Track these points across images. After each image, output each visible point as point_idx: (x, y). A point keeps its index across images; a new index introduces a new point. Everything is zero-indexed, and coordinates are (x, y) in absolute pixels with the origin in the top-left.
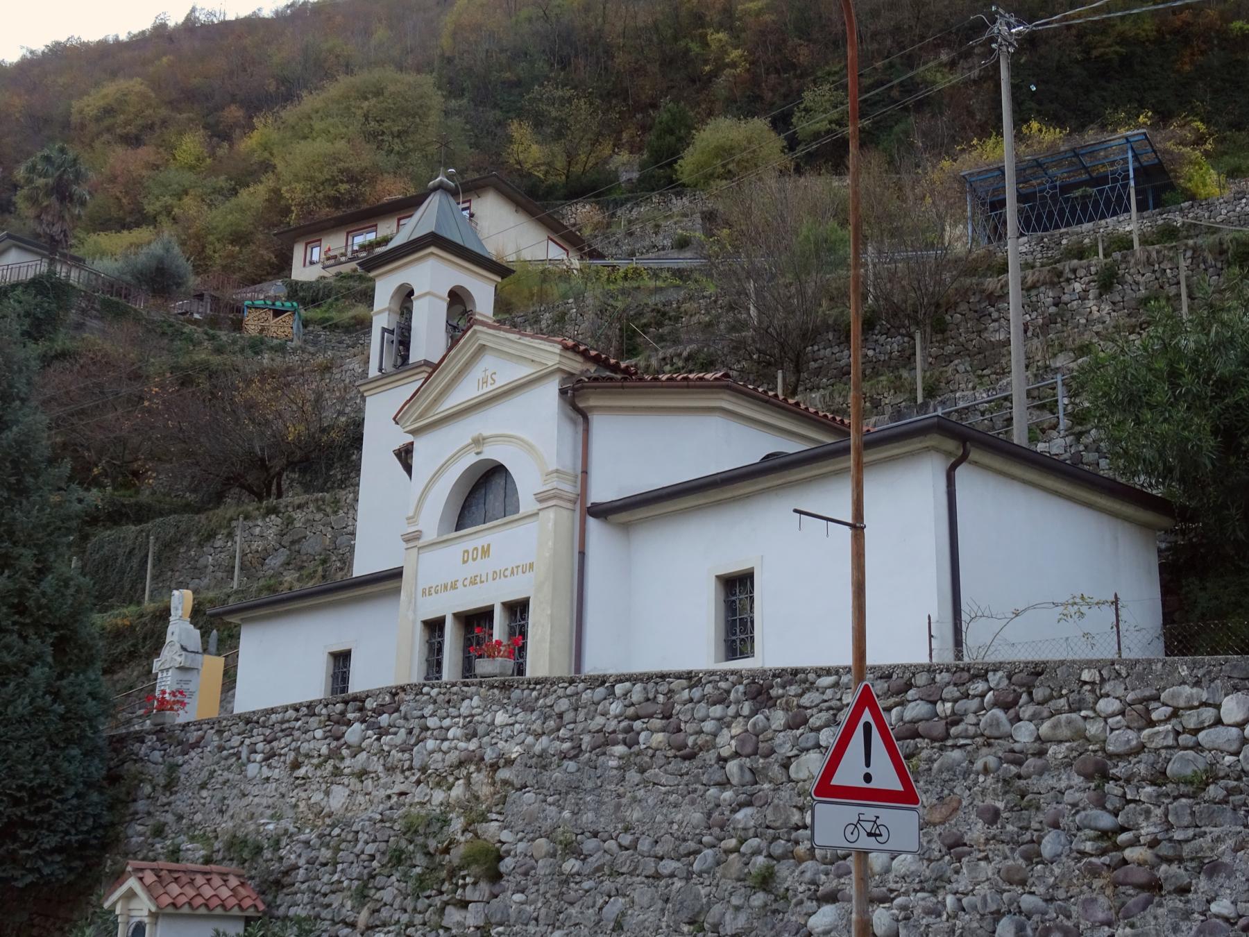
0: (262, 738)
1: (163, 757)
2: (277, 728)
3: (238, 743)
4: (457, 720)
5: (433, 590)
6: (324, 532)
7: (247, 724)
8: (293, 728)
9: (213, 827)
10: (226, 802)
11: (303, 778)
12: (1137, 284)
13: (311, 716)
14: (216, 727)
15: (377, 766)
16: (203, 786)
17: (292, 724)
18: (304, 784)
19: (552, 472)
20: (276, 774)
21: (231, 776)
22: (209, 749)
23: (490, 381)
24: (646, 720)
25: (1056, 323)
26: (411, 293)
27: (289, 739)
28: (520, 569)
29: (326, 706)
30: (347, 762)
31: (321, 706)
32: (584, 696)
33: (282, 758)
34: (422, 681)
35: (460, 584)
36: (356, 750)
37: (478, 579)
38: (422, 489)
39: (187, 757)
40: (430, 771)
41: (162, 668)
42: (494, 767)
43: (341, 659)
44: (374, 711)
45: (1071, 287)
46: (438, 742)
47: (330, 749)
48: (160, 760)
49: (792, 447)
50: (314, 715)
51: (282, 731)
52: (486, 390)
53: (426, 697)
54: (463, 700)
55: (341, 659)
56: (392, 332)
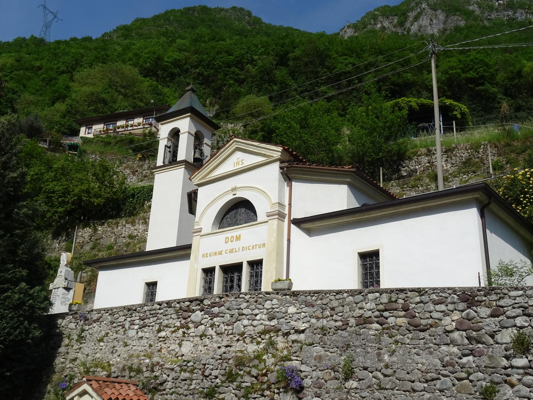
0: (138, 318)
1: (76, 326)
2: (148, 313)
3: (123, 320)
4: (262, 310)
5: (208, 255)
6: (111, 236)
7: (129, 311)
8: (157, 313)
9: (108, 360)
10: (115, 348)
11: (164, 338)
12: (462, 157)
13: (169, 308)
14: (110, 312)
15: (211, 332)
16: (101, 340)
17: (157, 312)
18: (164, 341)
19: (276, 203)
20: (147, 335)
21: (118, 336)
22: (105, 322)
23: (240, 163)
24: (392, 312)
25: (429, 170)
26: (179, 131)
27: (155, 319)
28: (257, 246)
29: (178, 303)
30: (192, 330)
31: (176, 303)
32: (347, 299)
33: (151, 328)
34: (247, 291)
35: (223, 253)
36: (197, 325)
37: (234, 250)
38: (203, 210)
39: (91, 326)
40: (246, 335)
41: (54, 287)
42: (287, 334)
43: (152, 286)
44: (209, 305)
45: (435, 156)
46: (250, 321)
47: (181, 324)
48: (75, 327)
49: (371, 202)
50: (171, 307)
51: (150, 314)
52: (238, 167)
53: (242, 299)
54: (266, 301)
55: (152, 286)
56: (169, 147)
